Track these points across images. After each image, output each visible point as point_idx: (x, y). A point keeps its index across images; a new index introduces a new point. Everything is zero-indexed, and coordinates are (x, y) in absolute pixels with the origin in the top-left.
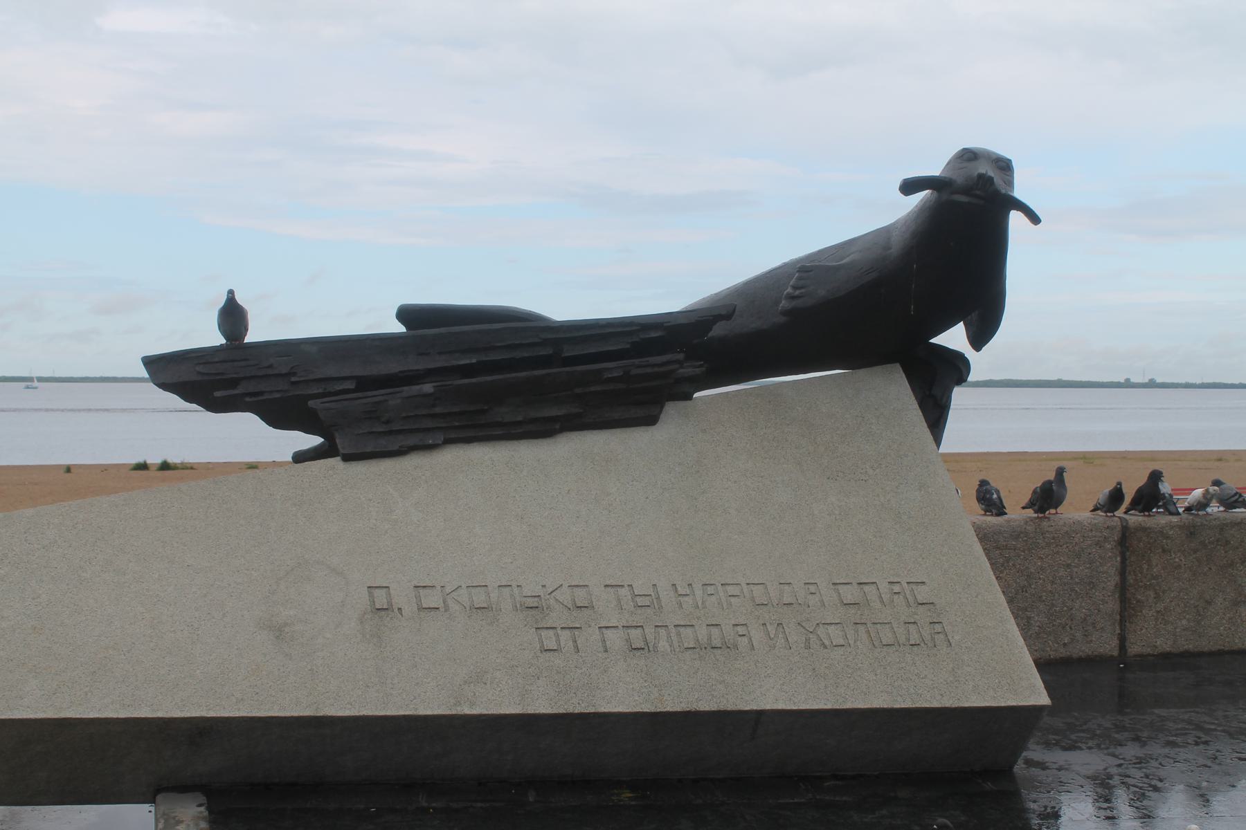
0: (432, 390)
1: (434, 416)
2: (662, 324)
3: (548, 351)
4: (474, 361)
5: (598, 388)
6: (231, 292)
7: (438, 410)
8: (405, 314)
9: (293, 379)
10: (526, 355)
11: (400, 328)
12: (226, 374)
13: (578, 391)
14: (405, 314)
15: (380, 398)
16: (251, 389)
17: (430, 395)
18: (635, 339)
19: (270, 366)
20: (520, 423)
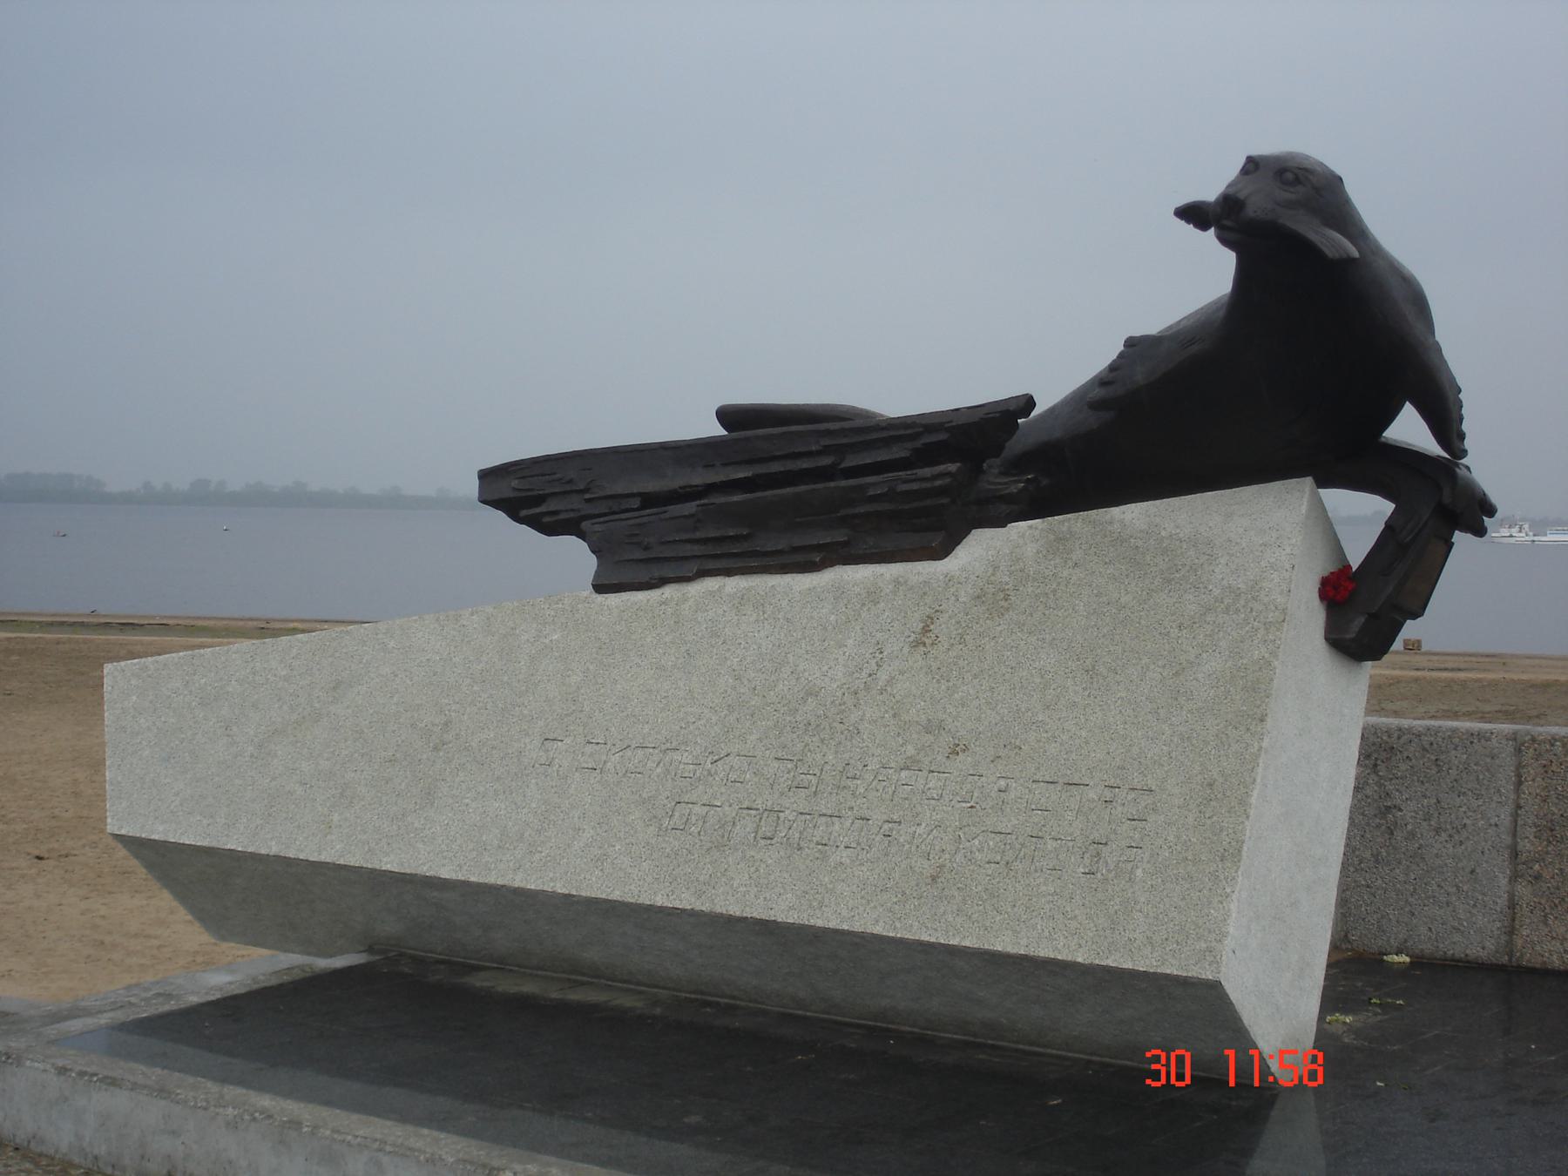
0: (694, 510)
1: (705, 541)
2: (942, 424)
3: (826, 461)
4: (749, 474)
5: (861, 510)
6: (1194, 214)
7: (698, 535)
8: (727, 416)
9: (587, 496)
10: (805, 466)
11: (720, 431)
12: (534, 493)
13: (843, 512)
14: (727, 416)
15: (645, 520)
16: (552, 508)
17: (692, 516)
18: (918, 444)
19: (570, 481)
20: (781, 552)
